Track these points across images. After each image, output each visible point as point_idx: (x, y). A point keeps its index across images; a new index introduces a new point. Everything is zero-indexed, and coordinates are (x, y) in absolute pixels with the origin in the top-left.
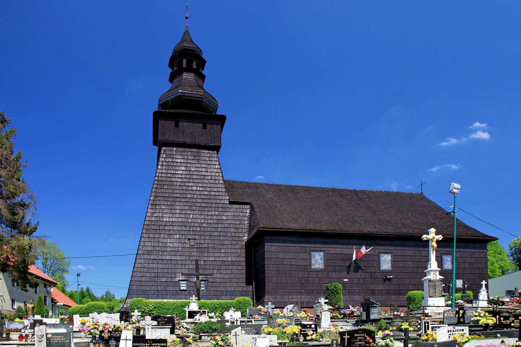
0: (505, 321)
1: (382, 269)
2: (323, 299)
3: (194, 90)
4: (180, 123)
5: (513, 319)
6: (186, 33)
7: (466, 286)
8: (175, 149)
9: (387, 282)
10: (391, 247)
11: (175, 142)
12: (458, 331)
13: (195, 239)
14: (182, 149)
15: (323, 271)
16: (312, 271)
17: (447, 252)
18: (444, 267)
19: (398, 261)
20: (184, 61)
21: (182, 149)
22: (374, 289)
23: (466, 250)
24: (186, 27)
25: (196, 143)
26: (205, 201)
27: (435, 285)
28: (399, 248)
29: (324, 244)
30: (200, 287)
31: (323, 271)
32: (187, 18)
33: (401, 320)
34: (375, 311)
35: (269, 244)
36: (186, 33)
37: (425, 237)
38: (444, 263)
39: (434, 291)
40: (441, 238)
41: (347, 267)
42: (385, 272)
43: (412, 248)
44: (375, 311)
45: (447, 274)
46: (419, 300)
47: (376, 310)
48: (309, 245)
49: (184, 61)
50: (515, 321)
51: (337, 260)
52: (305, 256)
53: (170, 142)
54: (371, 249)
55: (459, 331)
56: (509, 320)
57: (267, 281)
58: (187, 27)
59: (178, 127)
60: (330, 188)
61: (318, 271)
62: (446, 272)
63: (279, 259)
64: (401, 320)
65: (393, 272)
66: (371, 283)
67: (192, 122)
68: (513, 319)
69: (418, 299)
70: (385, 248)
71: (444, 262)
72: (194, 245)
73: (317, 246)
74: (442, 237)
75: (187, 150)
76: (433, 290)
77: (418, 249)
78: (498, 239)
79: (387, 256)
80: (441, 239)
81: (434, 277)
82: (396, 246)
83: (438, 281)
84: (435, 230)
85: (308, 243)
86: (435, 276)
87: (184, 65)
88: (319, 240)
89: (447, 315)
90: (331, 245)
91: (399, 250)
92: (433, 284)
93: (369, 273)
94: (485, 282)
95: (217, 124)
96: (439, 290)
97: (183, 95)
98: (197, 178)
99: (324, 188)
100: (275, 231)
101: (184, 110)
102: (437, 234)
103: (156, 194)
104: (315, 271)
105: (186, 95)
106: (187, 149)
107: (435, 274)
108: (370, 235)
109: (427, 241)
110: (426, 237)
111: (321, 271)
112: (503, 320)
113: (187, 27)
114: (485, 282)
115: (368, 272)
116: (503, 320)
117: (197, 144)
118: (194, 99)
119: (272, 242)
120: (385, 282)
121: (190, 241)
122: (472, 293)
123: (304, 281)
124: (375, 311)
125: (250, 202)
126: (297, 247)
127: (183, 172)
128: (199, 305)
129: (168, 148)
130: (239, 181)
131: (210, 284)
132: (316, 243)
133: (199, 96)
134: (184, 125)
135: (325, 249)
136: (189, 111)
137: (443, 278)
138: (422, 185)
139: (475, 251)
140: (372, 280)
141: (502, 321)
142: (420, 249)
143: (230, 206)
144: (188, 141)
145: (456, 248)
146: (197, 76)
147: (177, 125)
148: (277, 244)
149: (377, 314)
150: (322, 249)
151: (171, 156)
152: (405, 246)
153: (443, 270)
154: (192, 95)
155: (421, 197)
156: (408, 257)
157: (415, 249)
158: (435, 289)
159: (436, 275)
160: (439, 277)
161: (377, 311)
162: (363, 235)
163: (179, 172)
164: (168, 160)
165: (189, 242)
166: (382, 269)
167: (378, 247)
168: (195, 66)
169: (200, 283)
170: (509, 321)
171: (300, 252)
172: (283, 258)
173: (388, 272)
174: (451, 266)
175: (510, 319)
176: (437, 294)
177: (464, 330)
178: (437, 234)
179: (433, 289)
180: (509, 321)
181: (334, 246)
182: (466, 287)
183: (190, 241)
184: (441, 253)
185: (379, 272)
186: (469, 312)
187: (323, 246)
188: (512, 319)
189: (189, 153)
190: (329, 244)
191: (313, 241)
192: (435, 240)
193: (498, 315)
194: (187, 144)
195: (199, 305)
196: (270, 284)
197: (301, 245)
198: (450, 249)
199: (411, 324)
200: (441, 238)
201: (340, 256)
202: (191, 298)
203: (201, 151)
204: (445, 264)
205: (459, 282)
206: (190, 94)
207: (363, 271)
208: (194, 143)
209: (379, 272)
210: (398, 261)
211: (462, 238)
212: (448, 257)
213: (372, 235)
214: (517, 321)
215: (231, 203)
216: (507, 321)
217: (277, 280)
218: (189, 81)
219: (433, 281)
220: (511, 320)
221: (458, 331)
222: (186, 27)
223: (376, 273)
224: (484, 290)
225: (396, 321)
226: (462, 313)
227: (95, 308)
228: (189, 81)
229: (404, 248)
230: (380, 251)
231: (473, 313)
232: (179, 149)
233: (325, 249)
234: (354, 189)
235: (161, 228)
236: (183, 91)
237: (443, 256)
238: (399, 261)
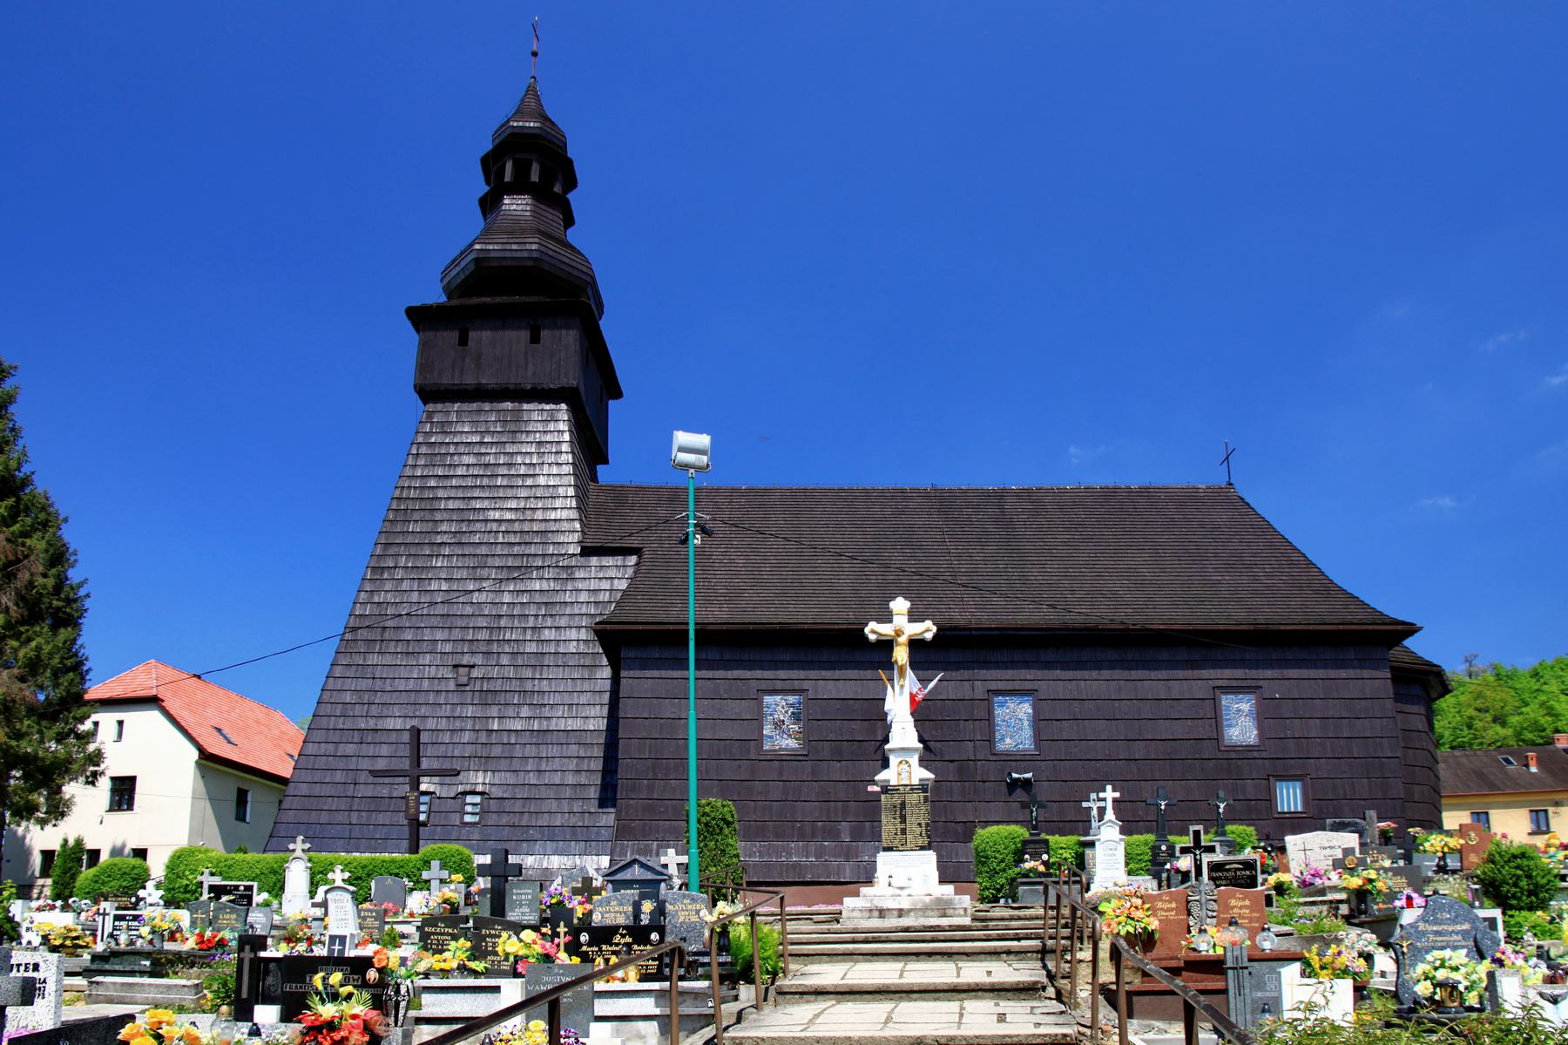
0: (597, 949)
1: (1000, 747)
2: (671, 851)
3: (511, 241)
4: (472, 334)
5: (630, 940)
6: (531, 90)
7: (1222, 806)
8: (456, 406)
9: (1020, 794)
10: (1031, 671)
11: (455, 388)
12: (18, 971)
13: (473, 666)
14: (475, 404)
15: (801, 758)
16: (762, 758)
17: (1235, 683)
18: (1226, 738)
19: (1056, 720)
20: (509, 166)
21: (474, 406)
22: (972, 820)
23: (1305, 673)
24: (532, 78)
25: (509, 385)
26: (516, 550)
27: (903, 804)
28: (1058, 673)
29: (803, 668)
30: (419, 812)
31: (801, 758)
32: (535, 54)
33: (450, 931)
34: (521, 894)
35: (632, 673)
36: (531, 90)
37: (875, 630)
38: (1225, 723)
39: (899, 827)
40: (927, 630)
41: (878, 744)
42: (1010, 758)
43: (1106, 674)
44: (521, 894)
45: (1240, 762)
46: (1002, 861)
47: (526, 891)
48: (759, 674)
49: (509, 166)
50: (635, 947)
51: (845, 722)
52: (742, 709)
53: (442, 388)
54: (939, 680)
55: (22, 968)
56: (611, 946)
57: (622, 793)
58: (535, 78)
59: (467, 345)
60: (924, 487)
61: (784, 758)
62: (1233, 755)
63: (662, 721)
64: (450, 931)
65: (1039, 758)
66: (960, 799)
67: (503, 328)
68: (630, 940)
69: (997, 855)
70: (1009, 674)
71: (1228, 720)
72: (468, 685)
73: (782, 674)
74: (934, 629)
75: (487, 406)
76: (894, 824)
77: (1125, 674)
78: (1421, 628)
79: (1020, 703)
80: (929, 636)
81: (904, 775)
82: (1048, 665)
83: (913, 788)
84: (907, 604)
85: (751, 665)
86: (908, 769)
87: (508, 178)
88: (787, 657)
89: (603, 917)
90: (824, 669)
91: (1059, 683)
92: (897, 800)
93: (956, 763)
94: (1114, 790)
95: (568, 327)
96: (920, 824)
97: (484, 256)
98: (505, 483)
99: (903, 491)
100: (638, 630)
101: (489, 297)
102: (914, 617)
103: (387, 539)
104: (774, 758)
105: (493, 255)
106: (487, 404)
107: (907, 762)
108: (948, 633)
109: (887, 645)
110: (873, 632)
111: (793, 758)
112: (590, 944)
113: (534, 77)
114: (1114, 790)
115: (952, 761)
116: (590, 944)
117: (511, 387)
118: (514, 263)
119: (643, 668)
120: (1010, 794)
121: (457, 673)
122: (1254, 833)
123: (738, 792)
124: (523, 897)
125: (640, 546)
126: (718, 681)
127: (467, 471)
128: (311, 869)
129: (439, 406)
130: (653, 485)
131: (493, 805)
132: (777, 665)
133: (526, 255)
134: (482, 338)
135: (806, 685)
136: (498, 300)
137: (932, 776)
138: (1227, 458)
139: (1343, 673)
140: (964, 787)
141: (584, 948)
142: (1135, 674)
143: (582, 561)
144: (488, 380)
145: (697, 668)
146: (540, 203)
147: (463, 341)
148: (656, 673)
149: (529, 905)
150: (796, 685)
151: (443, 426)
152: (1080, 665)
153: (1223, 749)
154: (508, 255)
155: (1227, 499)
156: (1090, 705)
157: (1117, 674)
158: (903, 820)
159: (910, 766)
160: (920, 774)
161: (530, 897)
162: (997, 633)
163: (460, 472)
164: (433, 440)
165: (455, 676)
166: (1000, 747)
167: (984, 671)
168: (535, 177)
169: (417, 799)
170: (610, 949)
171: (725, 696)
172: (673, 716)
173: (1022, 758)
174: (1255, 732)
175: (617, 939)
176: (909, 837)
177: (42, 966)
178: (914, 617)
179: (895, 818)
180: (610, 949)
181: (837, 674)
182: (1221, 810)
183: (457, 673)
184: (1214, 688)
185: (992, 758)
186: (683, 910)
187: (802, 674)
188: (623, 941)
189: (491, 413)
190: (820, 669)
191: (746, 657)
192: (903, 639)
193: (562, 924)
194: (487, 391)
195: (311, 869)
196: (631, 802)
197: (729, 672)
198: (1247, 671)
199: (486, 947)
200: (927, 630)
201: (857, 705)
202: (291, 846)
203: (525, 406)
204: (1230, 726)
205: (1291, 791)
206: (503, 252)
207: (936, 755)
208: (504, 386)
209: (992, 758)
210: (1056, 720)
211: (1280, 630)
212: (1241, 701)
213: (956, 633)
214: (642, 948)
215: (587, 552)
216: (604, 947)
217: (651, 788)
218: (546, 220)
219: (895, 789)
220: (617, 945)
221: (18, 971)
222: (532, 78)
223: (979, 763)
224: (1110, 821)
225: (434, 934)
226: (648, 911)
227: (110, 876)
228: (546, 220)
229: (1078, 674)
230: (994, 686)
231: (698, 912)
232: (466, 406)
233: (1042, 685)
234: (1002, 487)
235: (386, 636)
236: (484, 247)
237: (1223, 697)
238: (1059, 720)
